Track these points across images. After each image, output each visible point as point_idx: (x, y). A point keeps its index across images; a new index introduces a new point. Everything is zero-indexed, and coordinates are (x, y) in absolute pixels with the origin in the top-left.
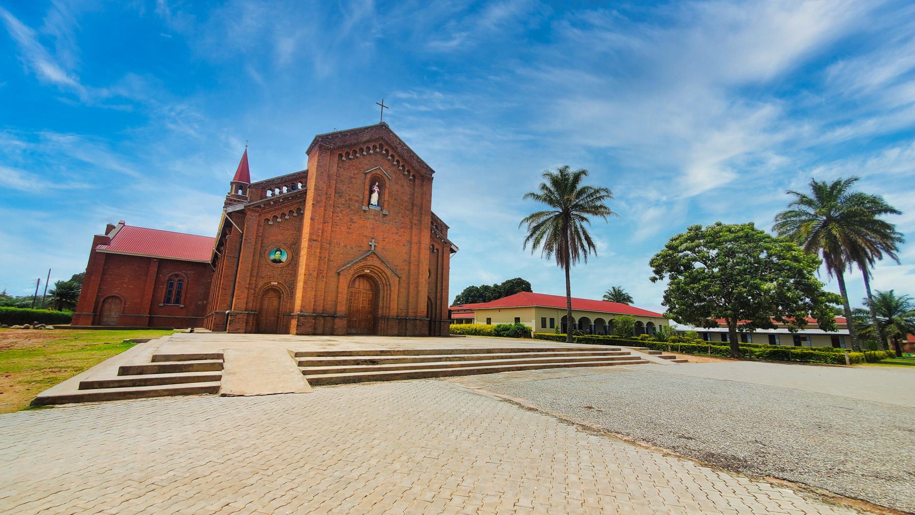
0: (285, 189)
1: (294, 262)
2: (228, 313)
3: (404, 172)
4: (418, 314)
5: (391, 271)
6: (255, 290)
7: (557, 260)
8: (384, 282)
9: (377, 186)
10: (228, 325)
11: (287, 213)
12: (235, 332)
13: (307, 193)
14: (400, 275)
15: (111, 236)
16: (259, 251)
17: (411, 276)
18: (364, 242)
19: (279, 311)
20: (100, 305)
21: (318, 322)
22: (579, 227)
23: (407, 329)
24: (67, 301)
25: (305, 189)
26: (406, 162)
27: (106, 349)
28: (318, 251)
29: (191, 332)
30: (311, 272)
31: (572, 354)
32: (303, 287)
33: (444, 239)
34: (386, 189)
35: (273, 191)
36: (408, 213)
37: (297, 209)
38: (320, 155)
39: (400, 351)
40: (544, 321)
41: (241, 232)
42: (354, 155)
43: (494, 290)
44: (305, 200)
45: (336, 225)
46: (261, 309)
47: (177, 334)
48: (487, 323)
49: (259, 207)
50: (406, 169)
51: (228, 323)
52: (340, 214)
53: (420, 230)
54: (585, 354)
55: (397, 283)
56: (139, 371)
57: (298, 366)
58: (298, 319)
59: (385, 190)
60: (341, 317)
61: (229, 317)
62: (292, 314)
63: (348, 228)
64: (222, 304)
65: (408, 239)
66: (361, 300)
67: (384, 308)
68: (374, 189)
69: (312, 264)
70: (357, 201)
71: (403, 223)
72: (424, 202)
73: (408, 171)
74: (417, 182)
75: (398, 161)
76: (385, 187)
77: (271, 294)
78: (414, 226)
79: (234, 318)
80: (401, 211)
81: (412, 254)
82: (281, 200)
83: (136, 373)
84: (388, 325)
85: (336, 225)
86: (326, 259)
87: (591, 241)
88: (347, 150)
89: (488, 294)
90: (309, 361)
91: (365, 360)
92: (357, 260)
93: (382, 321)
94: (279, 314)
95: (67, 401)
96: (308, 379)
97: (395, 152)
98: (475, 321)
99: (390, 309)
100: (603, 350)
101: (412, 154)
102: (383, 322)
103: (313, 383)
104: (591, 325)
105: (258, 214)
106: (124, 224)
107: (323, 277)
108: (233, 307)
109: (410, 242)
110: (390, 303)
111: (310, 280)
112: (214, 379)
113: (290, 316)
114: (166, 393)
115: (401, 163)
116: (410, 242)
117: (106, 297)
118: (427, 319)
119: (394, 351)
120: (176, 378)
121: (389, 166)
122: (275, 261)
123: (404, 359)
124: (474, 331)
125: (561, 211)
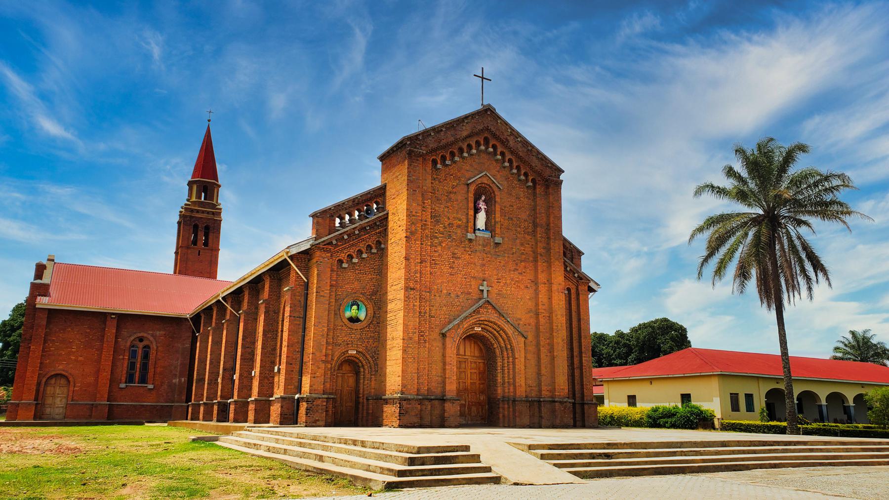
1: (378, 320)
2: (298, 398)
4: (556, 394)
7: (760, 292)
8: (503, 345)
9: (484, 201)
11: (364, 250)
12: (314, 424)
15: (46, 280)
18: (473, 287)
20: (42, 389)
22: (794, 238)
23: (541, 417)
26: (521, 161)
28: (417, 304)
30: (411, 335)
31: (834, 449)
32: (403, 358)
33: (578, 272)
34: (497, 206)
36: (528, 237)
37: (377, 241)
38: (409, 165)
40: (734, 398)
41: (306, 281)
43: (617, 343)
45: (435, 264)
48: (629, 405)
49: (330, 243)
50: (523, 172)
52: (439, 248)
53: (550, 266)
54: (851, 449)
55: (523, 345)
58: (400, 404)
60: (452, 400)
62: (383, 397)
64: (288, 385)
65: (532, 278)
67: (506, 385)
68: (480, 206)
69: (412, 323)
70: (459, 226)
71: (522, 254)
72: (552, 219)
73: (526, 175)
74: (540, 190)
75: (510, 161)
76: (495, 202)
78: (539, 257)
79: (311, 406)
80: (518, 235)
81: (540, 300)
82: (357, 232)
84: (514, 411)
85: (435, 264)
87: (818, 261)
88: (442, 152)
90: (549, 454)
98: (606, 401)
100: (874, 444)
101: (530, 148)
102: (506, 406)
104: (820, 406)
105: (329, 255)
106: (53, 260)
109: (535, 282)
110: (514, 377)
111: (411, 347)
112: (486, 470)
113: (380, 400)
114: (464, 482)
117: (49, 375)
119: (621, 444)
124: (608, 419)
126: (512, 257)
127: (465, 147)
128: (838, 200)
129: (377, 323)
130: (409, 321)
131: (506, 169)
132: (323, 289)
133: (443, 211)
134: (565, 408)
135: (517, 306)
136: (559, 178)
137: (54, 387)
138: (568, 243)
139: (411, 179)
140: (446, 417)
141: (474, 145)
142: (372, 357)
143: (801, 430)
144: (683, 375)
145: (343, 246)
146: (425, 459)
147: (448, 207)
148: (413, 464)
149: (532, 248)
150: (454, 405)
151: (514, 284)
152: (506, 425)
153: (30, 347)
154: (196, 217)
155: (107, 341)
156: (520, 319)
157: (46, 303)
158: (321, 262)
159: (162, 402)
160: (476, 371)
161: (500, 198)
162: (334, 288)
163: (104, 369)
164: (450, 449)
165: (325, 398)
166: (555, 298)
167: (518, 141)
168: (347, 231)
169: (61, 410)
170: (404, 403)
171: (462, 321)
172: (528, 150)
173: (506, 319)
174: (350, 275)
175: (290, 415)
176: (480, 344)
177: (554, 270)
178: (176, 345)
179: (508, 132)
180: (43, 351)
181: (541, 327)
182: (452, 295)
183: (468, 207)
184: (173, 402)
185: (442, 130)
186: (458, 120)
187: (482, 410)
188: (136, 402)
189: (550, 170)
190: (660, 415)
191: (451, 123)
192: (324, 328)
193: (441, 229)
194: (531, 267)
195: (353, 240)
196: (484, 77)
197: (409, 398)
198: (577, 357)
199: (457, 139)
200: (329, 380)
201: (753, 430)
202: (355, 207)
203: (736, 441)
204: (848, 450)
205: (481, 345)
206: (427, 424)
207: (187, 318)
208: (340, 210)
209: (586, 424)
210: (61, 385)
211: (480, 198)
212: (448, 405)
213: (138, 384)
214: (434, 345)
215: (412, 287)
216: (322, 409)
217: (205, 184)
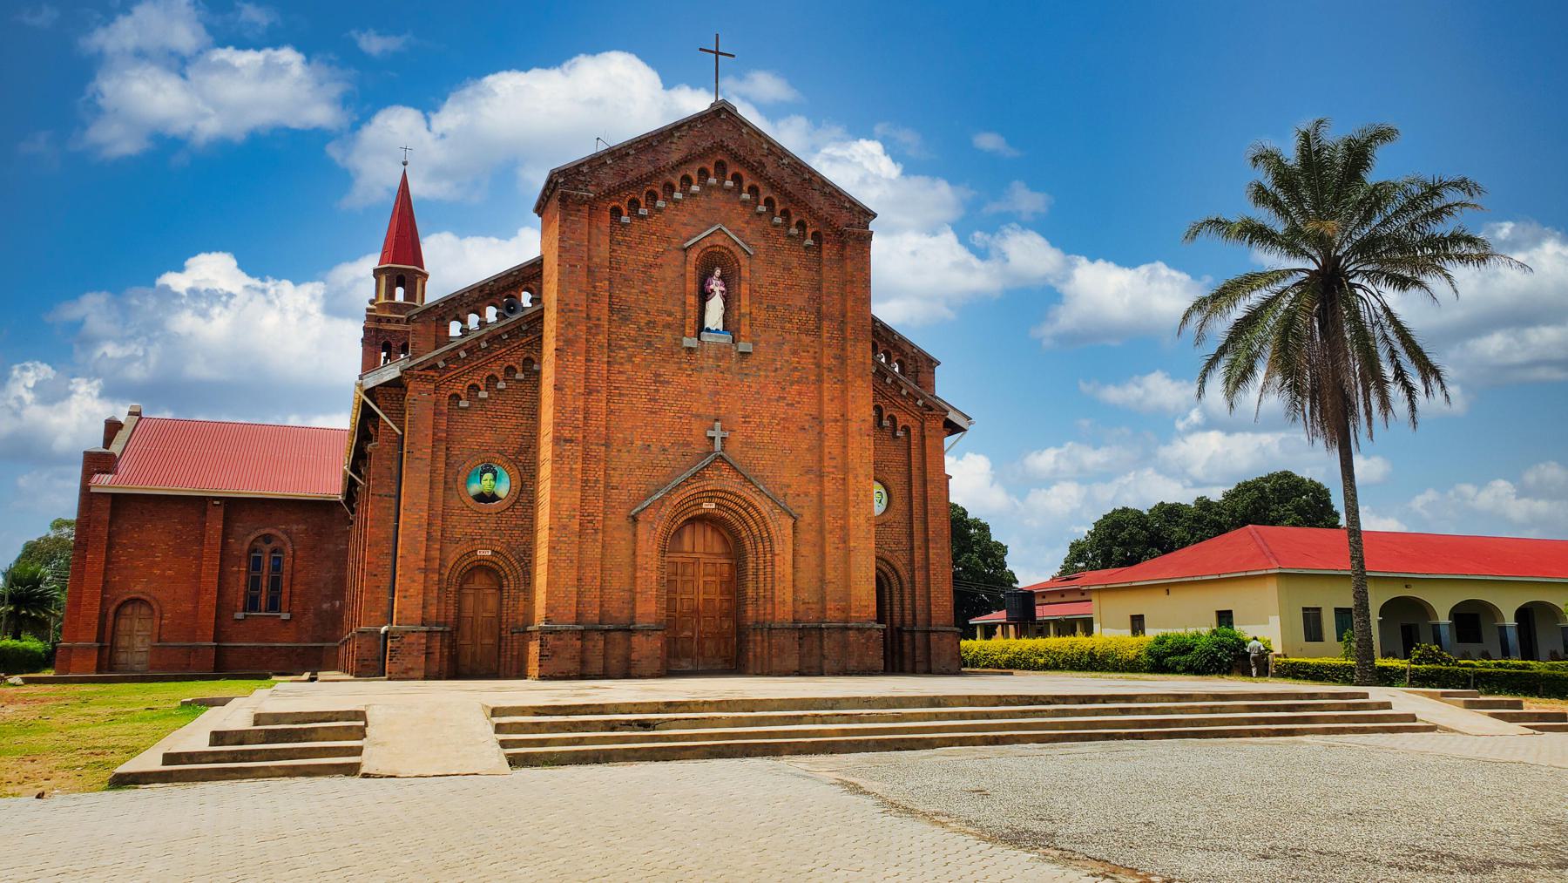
0: (491, 313)
2: (386, 632)
3: (789, 228)
4: (853, 615)
5: (769, 501)
6: (440, 574)
8: (756, 532)
10: (387, 661)
12: (404, 676)
13: (545, 319)
14: (796, 511)
16: (441, 478)
17: (827, 511)
19: (500, 623)
20: (110, 623)
21: (589, 644)
24: (29, 614)
25: (538, 307)
27: (153, 718)
28: (578, 466)
29: (312, 680)
32: (549, 561)
33: (923, 397)
35: (464, 322)
36: (806, 339)
38: (563, 220)
39: (710, 703)
41: (400, 433)
42: (650, 203)
44: (542, 336)
46: (459, 617)
47: (283, 684)
49: (434, 367)
50: (794, 221)
51: (388, 656)
52: (628, 367)
56: (238, 739)
57: (496, 733)
58: (541, 639)
59: (739, 285)
60: (647, 631)
61: (389, 641)
62: (529, 628)
63: (650, 400)
64: (371, 611)
66: (701, 582)
67: (762, 600)
68: (712, 287)
70: (668, 326)
72: (850, 304)
74: (828, 251)
75: (769, 202)
76: (740, 277)
77: (480, 581)
78: (826, 374)
80: (788, 337)
81: (826, 450)
82: (484, 345)
83: (233, 742)
85: (620, 395)
86: (601, 485)
88: (633, 194)
89: (1178, 532)
90: (515, 723)
91: (627, 721)
92: (678, 481)
93: (756, 636)
94: (501, 629)
95: (152, 780)
96: (507, 755)
97: (761, 177)
99: (774, 604)
102: (759, 638)
103: (514, 761)
104: (1503, 629)
107: (596, 531)
108: (395, 617)
111: (565, 542)
112: (350, 752)
113: (524, 633)
114: (281, 772)
115: (777, 207)
116: (818, 419)
117: (120, 600)
118: (879, 626)
119: (696, 703)
120: (293, 749)
121: (747, 217)
122: (482, 498)
123: (713, 719)
124: (1086, 659)
125: (1314, 267)
126: (774, 377)
127: (677, 182)
128: (1465, 234)
129: (529, 502)
130: (561, 497)
131: (763, 217)
132: (419, 447)
133: (638, 300)
134: (868, 641)
135: (782, 462)
136: (868, 227)
137: (131, 619)
138: (907, 346)
139: (567, 245)
140: (634, 660)
141: (695, 178)
142: (520, 560)
143: (1408, 673)
144: (1217, 577)
145: (458, 371)
146: (247, 735)
147: (646, 293)
148: (220, 743)
149: (815, 358)
150: (650, 638)
151: (777, 424)
152: (758, 672)
153: (86, 557)
154: (386, 331)
155: (209, 544)
156: (788, 486)
157: (107, 483)
158: (415, 400)
159: (306, 642)
160: (714, 578)
161: (754, 273)
162: (444, 444)
163: (206, 590)
164: (322, 718)
165: (423, 632)
166: (854, 446)
167: (783, 164)
168: (465, 344)
169: (144, 657)
170: (550, 637)
171: (668, 493)
172: (805, 180)
173: (756, 487)
174: (477, 419)
175: (372, 660)
176: (723, 532)
177: (853, 397)
178: (326, 546)
179: (763, 148)
180: (108, 562)
181: (826, 498)
182: (653, 448)
183: (685, 290)
184: (324, 640)
185: (628, 154)
186: (662, 133)
187: (726, 647)
188: (263, 642)
189: (848, 214)
190: (1169, 651)
191: (646, 139)
192: (421, 513)
193: (632, 333)
194: (813, 392)
195: (479, 359)
196: (720, 51)
197: (558, 629)
198: (920, 548)
199: (660, 168)
200: (435, 602)
201: (1326, 675)
202: (485, 300)
203: (963, 697)
204: (1214, 710)
205: (726, 534)
206: (598, 673)
207: (339, 502)
208: (456, 307)
209: (934, 667)
210: (141, 617)
211: (712, 275)
212: (637, 640)
213: (266, 612)
214: (616, 536)
215: (568, 438)
216: (418, 651)
217: (399, 273)
